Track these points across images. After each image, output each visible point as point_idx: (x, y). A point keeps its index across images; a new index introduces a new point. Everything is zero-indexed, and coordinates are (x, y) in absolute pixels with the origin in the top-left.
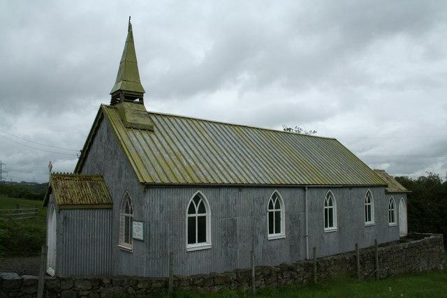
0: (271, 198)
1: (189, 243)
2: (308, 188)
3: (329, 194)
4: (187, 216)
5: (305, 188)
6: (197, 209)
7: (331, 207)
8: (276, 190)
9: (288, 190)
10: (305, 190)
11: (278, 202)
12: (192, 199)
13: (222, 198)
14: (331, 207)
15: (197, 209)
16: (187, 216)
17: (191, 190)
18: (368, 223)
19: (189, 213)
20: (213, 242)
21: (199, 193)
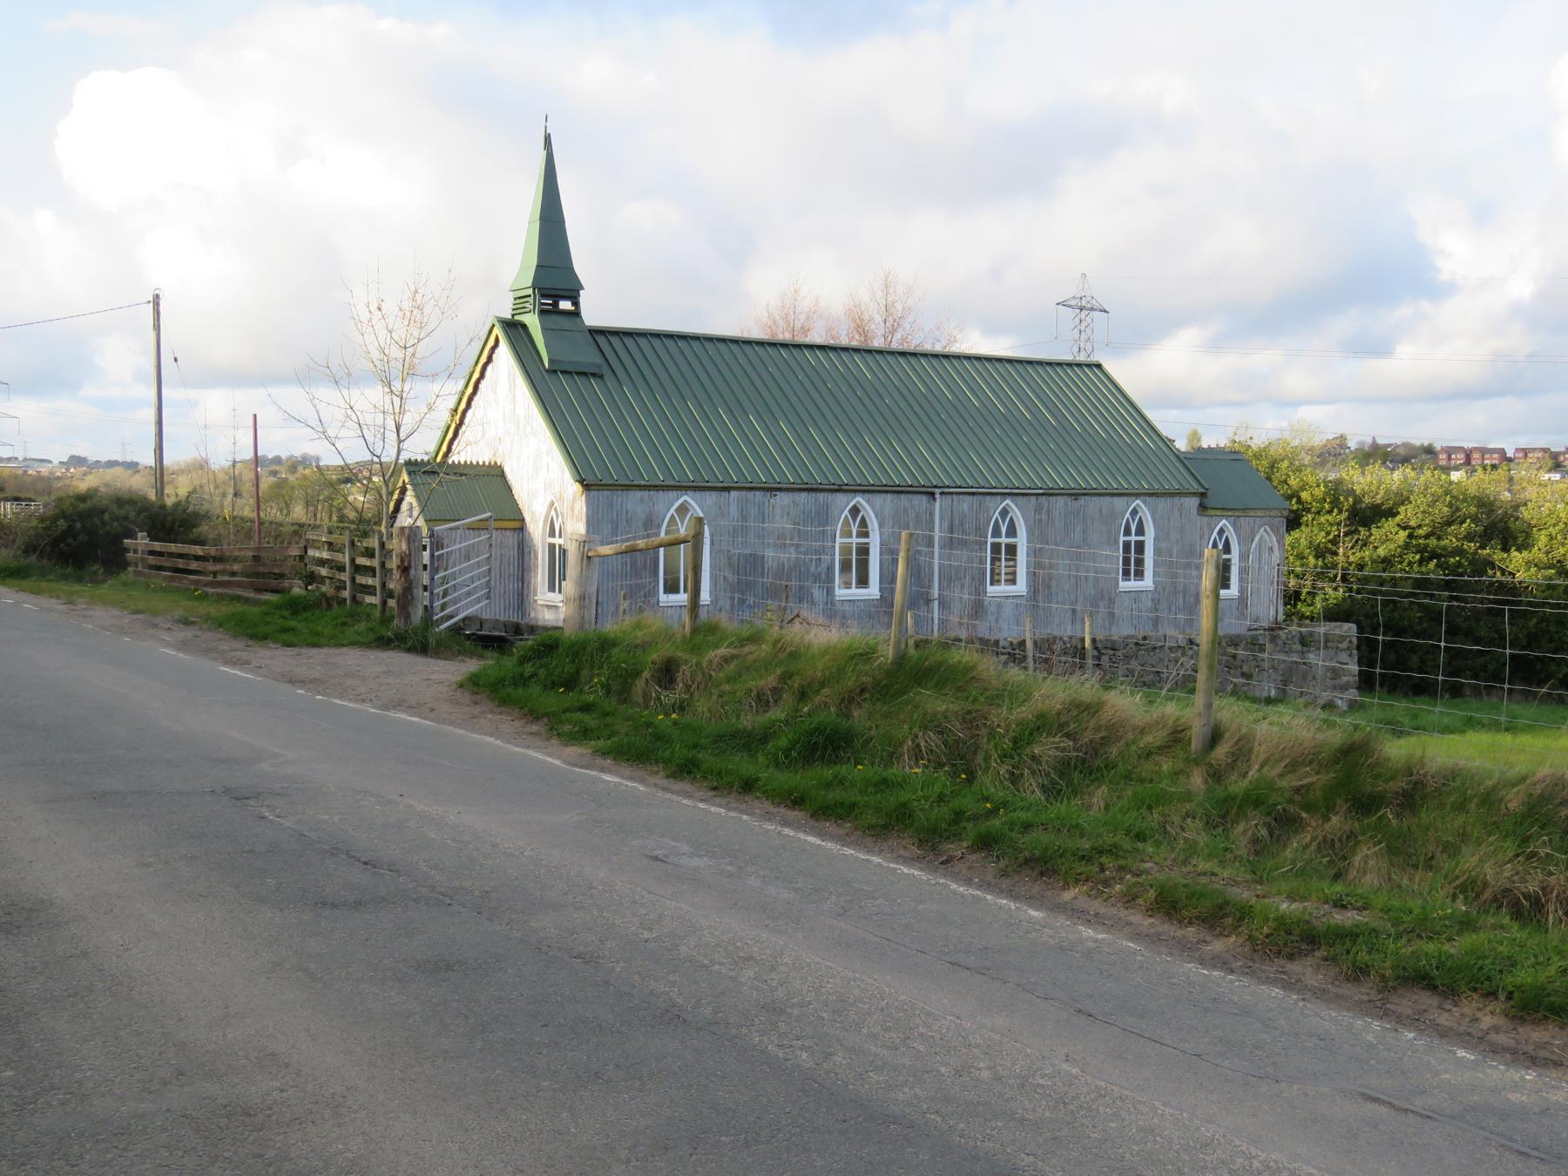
0: (1128, 515)
1: (665, 592)
2: (942, 493)
3: (855, 511)
4: (139, 541)
5: (933, 494)
6: (1004, 530)
7: (1140, 538)
8: (686, 498)
9: (878, 495)
10: (934, 499)
11: (863, 523)
12: (672, 511)
13: (734, 510)
14: (1140, 538)
15: (1004, 530)
16: (990, 540)
17: (672, 494)
18: (856, 593)
19: (1124, 535)
20: (1029, 585)
21: (1138, 505)
